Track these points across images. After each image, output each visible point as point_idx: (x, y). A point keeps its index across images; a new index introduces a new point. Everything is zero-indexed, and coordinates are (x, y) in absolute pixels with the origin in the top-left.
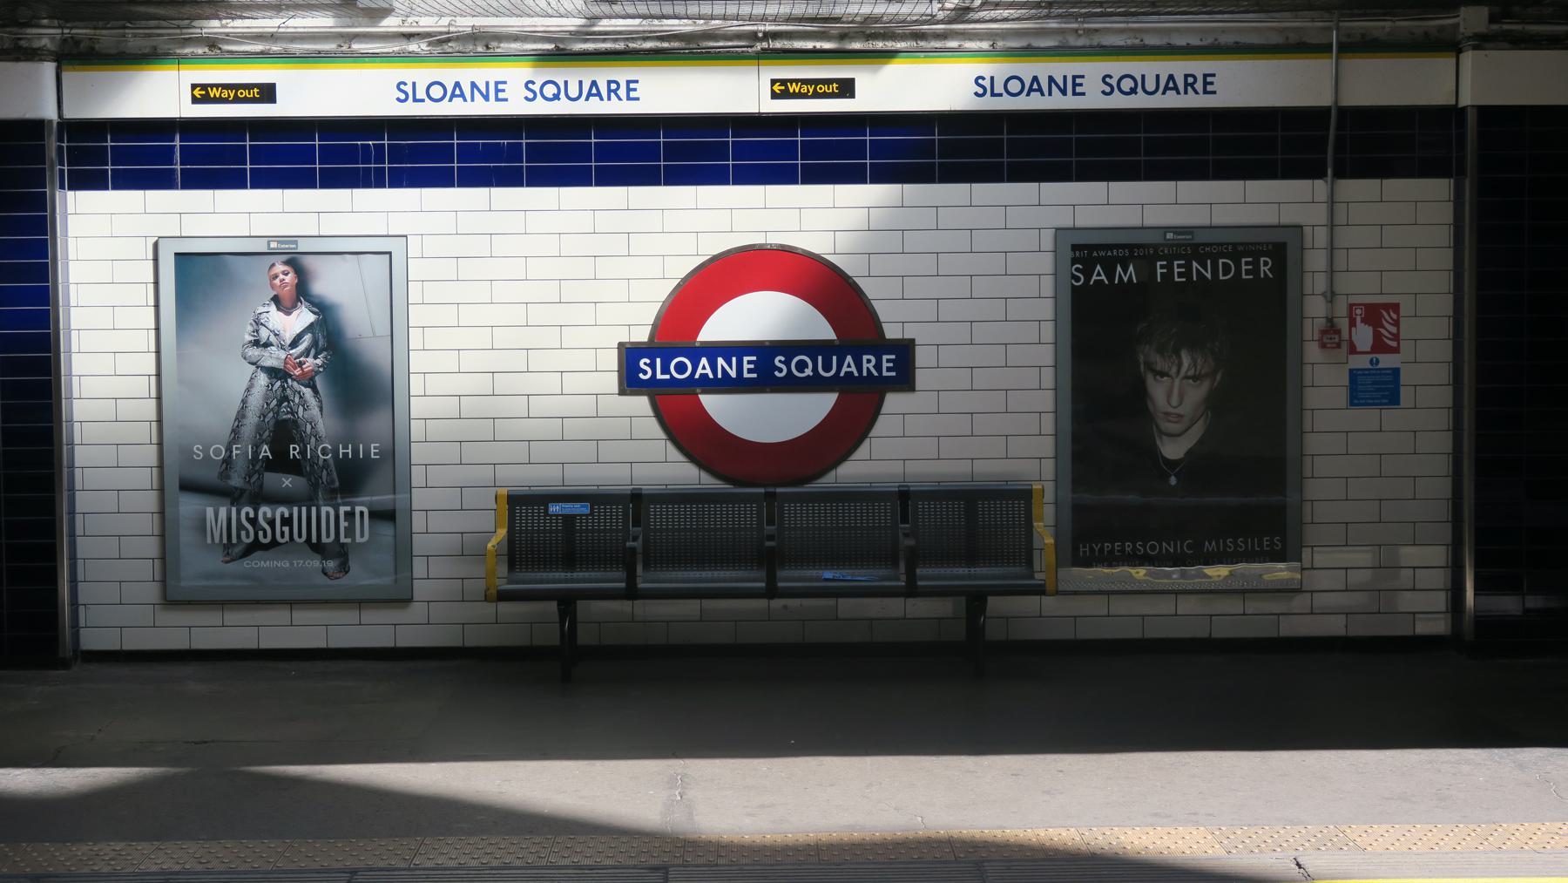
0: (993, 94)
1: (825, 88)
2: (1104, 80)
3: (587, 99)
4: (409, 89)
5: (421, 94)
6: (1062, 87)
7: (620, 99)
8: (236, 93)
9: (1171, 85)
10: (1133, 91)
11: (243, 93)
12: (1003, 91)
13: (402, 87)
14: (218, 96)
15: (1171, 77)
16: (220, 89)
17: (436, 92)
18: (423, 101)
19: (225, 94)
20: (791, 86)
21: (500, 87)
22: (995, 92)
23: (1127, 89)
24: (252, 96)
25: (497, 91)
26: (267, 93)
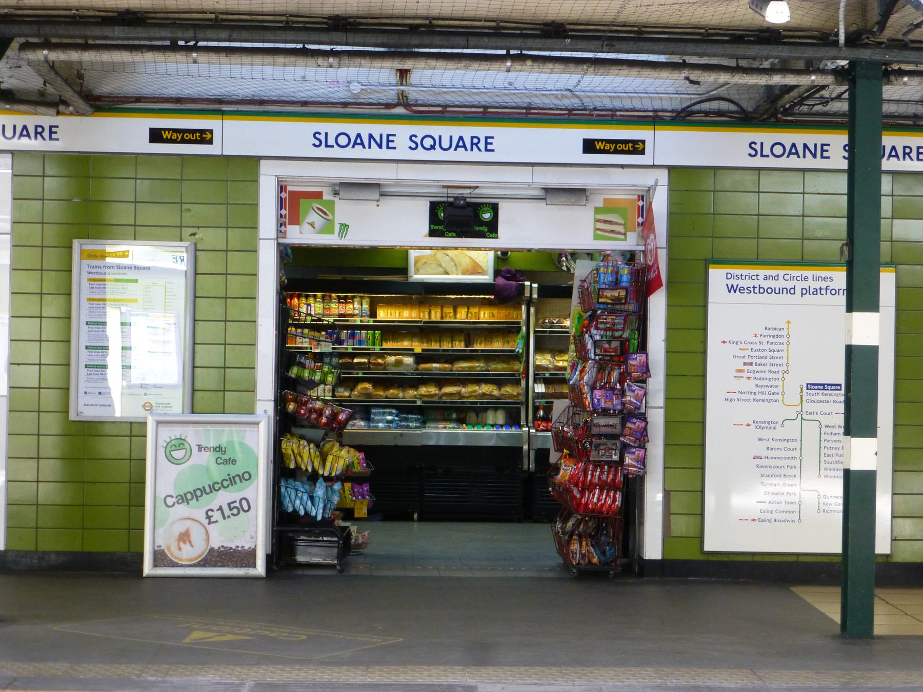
0: (327, 146)
1: (190, 136)
2: (411, 139)
3: (455, 150)
4: (322, 137)
5: (767, 151)
6: (379, 143)
7: (480, 150)
8: (183, 136)
9: (461, 144)
10: (433, 147)
11: (188, 136)
12: (333, 143)
13: (317, 135)
14: (602, 148)
15: (461, 138)
16: (171, 132)
17: (343, 140)
18: (332, 146)
19: (175, 136)
20: (165, 133)
21: (391, 138)
22: (764, 154)
23: (427, 146)
24: (627, 149)
25: (388, 141)
26: (156, 136)
